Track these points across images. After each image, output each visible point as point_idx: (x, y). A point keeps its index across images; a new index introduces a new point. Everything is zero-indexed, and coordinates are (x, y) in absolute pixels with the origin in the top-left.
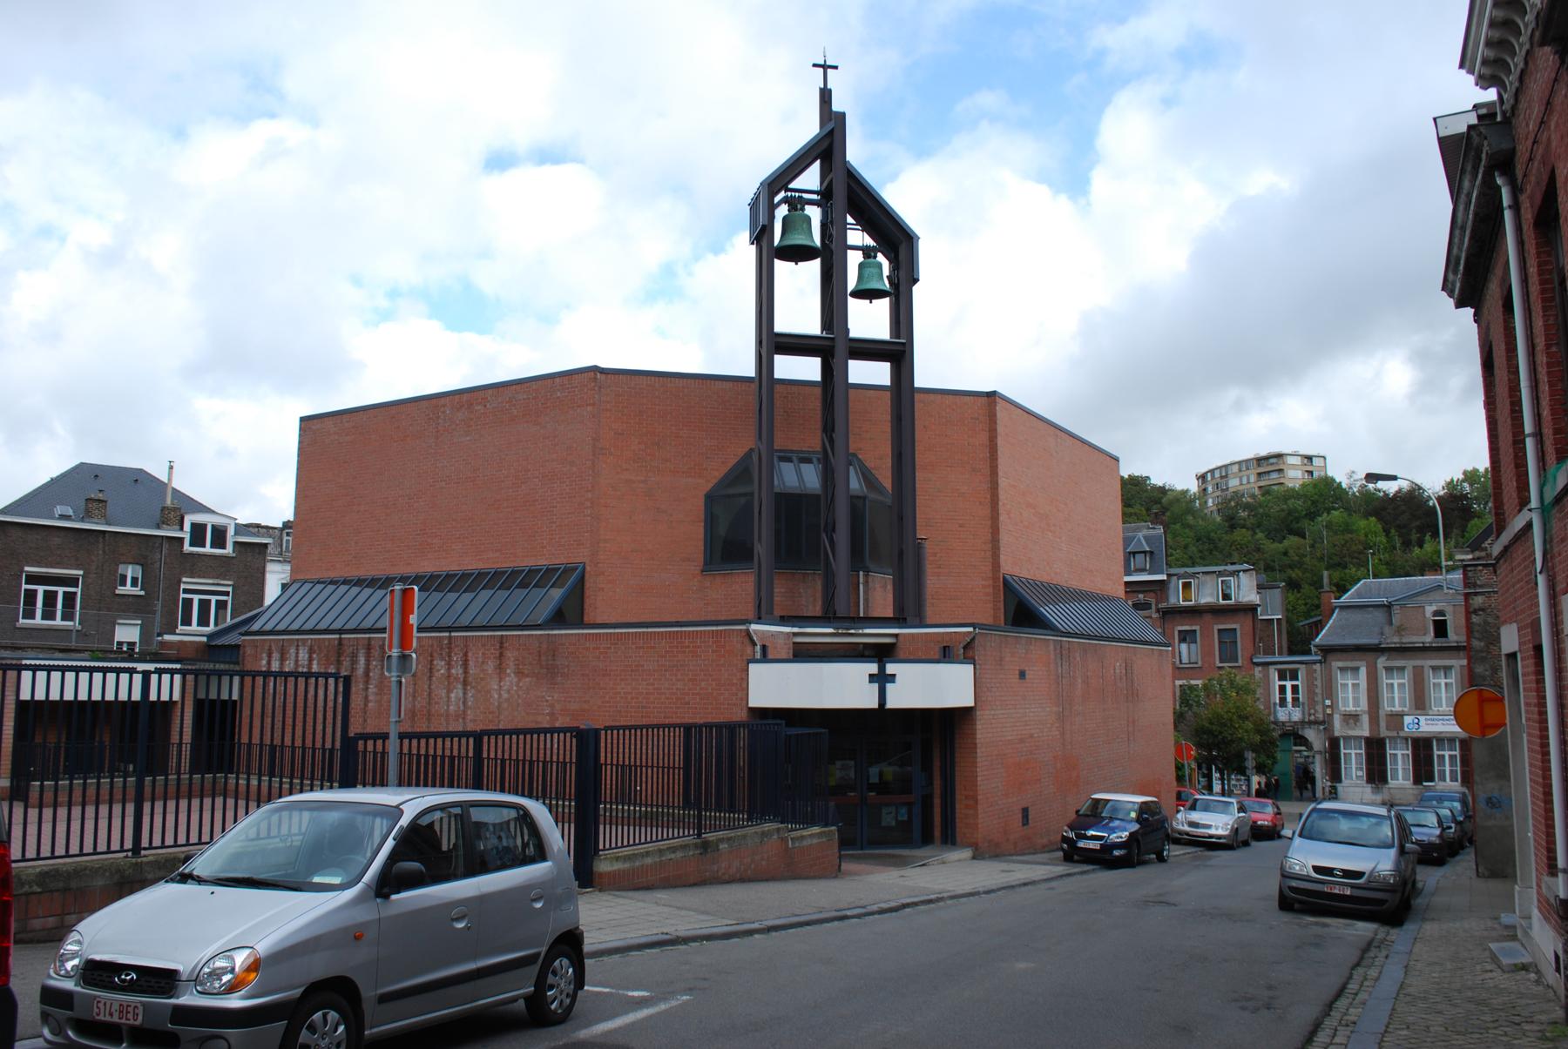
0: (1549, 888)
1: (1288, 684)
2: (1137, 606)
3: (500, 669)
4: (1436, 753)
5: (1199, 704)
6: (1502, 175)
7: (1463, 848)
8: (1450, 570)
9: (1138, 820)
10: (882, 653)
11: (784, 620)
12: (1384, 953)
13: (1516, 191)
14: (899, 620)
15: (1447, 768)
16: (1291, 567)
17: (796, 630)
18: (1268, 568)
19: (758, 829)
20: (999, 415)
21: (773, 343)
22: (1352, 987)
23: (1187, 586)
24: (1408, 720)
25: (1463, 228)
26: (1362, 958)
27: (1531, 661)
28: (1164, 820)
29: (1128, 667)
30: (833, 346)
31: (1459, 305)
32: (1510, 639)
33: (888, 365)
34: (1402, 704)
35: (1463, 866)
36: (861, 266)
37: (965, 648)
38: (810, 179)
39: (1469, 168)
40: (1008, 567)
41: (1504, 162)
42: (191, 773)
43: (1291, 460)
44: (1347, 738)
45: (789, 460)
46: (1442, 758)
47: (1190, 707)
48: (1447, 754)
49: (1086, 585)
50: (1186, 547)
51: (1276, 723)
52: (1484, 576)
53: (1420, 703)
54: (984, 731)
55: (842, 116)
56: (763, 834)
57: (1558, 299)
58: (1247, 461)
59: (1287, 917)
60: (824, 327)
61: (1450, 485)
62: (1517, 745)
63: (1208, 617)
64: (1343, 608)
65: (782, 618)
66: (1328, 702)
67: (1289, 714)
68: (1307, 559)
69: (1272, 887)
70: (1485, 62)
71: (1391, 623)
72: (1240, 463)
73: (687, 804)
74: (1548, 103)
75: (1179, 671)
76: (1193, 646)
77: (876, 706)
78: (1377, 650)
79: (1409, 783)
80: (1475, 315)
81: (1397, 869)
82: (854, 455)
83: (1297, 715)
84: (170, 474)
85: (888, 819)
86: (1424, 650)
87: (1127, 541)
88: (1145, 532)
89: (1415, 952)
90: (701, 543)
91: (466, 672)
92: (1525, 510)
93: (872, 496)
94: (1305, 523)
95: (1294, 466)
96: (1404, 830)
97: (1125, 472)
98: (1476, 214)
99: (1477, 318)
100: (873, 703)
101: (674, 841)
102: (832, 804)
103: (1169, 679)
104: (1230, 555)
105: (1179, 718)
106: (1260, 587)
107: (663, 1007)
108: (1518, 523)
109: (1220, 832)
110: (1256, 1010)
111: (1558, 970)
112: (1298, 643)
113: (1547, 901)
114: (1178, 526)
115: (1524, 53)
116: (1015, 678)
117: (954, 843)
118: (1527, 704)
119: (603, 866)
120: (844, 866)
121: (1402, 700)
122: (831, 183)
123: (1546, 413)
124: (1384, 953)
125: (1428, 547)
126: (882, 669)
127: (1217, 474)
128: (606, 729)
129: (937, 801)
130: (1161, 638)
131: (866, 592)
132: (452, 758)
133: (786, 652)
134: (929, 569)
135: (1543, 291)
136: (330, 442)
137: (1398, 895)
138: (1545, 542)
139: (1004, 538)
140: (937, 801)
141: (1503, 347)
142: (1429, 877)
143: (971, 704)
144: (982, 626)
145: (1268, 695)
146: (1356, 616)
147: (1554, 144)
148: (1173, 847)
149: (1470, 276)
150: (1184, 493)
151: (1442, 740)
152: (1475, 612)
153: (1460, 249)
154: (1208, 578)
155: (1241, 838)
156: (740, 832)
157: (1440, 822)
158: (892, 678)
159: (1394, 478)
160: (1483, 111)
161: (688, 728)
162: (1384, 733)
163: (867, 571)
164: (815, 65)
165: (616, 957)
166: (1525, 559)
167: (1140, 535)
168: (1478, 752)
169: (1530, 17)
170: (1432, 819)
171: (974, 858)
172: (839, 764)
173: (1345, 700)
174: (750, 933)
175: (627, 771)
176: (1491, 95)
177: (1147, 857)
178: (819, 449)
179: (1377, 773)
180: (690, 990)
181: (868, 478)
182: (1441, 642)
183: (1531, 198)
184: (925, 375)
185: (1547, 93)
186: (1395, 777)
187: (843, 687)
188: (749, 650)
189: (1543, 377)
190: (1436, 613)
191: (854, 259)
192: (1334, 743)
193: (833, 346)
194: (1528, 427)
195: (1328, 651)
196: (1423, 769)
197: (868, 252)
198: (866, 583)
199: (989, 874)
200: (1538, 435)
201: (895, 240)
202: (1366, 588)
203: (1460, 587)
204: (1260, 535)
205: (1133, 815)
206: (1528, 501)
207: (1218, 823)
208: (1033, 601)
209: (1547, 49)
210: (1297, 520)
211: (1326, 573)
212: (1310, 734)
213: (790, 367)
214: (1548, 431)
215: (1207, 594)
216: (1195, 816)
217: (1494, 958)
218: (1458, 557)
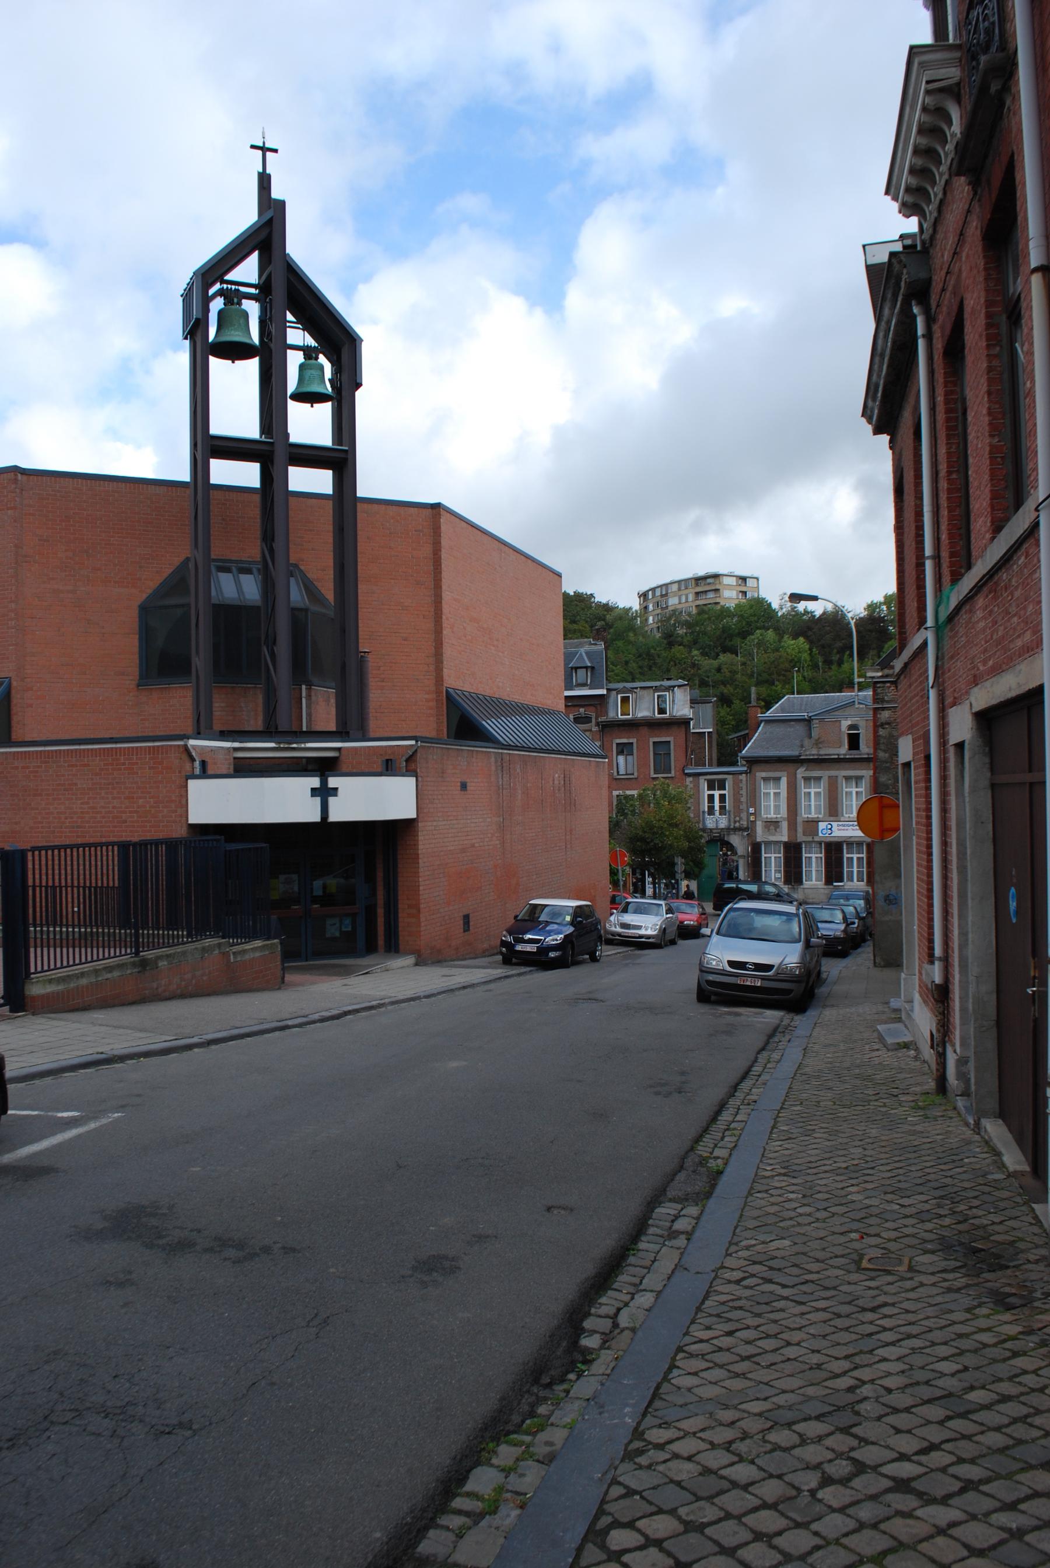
0: (927, 974)
1: (717, 794)
2: (578, 720)
4: (846, 855)
5: (633, 812)
6: (919, 303)
7: (864, 941)
8: (862, 687)
9: (572, 923)
10: (325, 767)
11: (223, 735)
12: (787, 1037)
13: (930, 321)
15: (855, 870)
17: (236, 745)
18: (703, 684)
19: (198, 945)
20: (443, 528)
21: (208, 446)
22: (757, 1069)
23: (625, 700)
24: (822, 825)
25: (882, 356)
26: (767, 1043)
27: (922, 770)
28: (598, 922)
29: (566, 777)
30: (272, 450)
31: (877, 431)
32: (906, 750)
33: (330, 472)
34: (818, 811)
35: (863, 957)
36: (302, 367)
37: (407, 761)
38: (248, 271)
39: (889, 296)
40: (451, 681)
41: (920, 292)
43: (726, 581)
44: (768, 843)
45: (228, 570)
47: (625, 815)
48: (855, 856)
49: (528, 698)
50: (627, 663)
51: (704, 830)
52: (890, 693)
53: (834, 811)
54: (426, 842)
55: (282, 204)
56: (204, 950)
57: (960, 428)
58: (686, 580)
59: (705, 1008)
60: (263, 431)
61: (872, 607)
62: (908, 847)
63: (644, 731)
64: (768, 722)
66: (752, 810)
67: (716, 822)
68: (739, 676)
69: (691, 981)
70: (908, 190)
71: (810, 736)
72: (679, 582)
73: (125, 924)
74: (961, 234)
75: (616, 781)
76: (630, 758)
78: (796, 761)
79: (821, 884)
80: (891, 442)
81: (803, 962)
82: (296, 566)
85: (332, 929)
86: (839, 761)
87: (568, 657)
88: (587, 648)
89: (815, 1034)
90: (137, 656)
92: (922, 630)
93: (315, 608)
94: (737, 641)
95: (729, 587)
96: (810, 925)
97: (570, 587)
98: (894, 342)
99: (892, 445)
100: (316, 817)
101: (109, 961)
102: (274, 917)
103: (605, 792)
104: (668, 670)
105: (614, 827)
106: (693, 702)
107: (92, 1125)
108: (916, 642)
109: (649, 932)
110: (668, 1095)
111: (932, 1047)
112: (727, 755)
113: (926, 986)
114: (620, 643)
115: (943, 182)
118: (917, 809)
119: (35, 989)
120: (288, 977)
121: (818, 807)
122: (269, 277)
123: (944, 537)
124: (787, 1037)
125: (846, 666)
126: (324, 783)
127: (658, 593)
128: (33, 849)
129: (380, 911)
130: (600, 752)
131: (308, 706)
133: (227, 767)
134: (372, 683)
135: (948, 420)
137: (803, 985)
138: (937, 659)
139: (448, 652)
140: (380, 911)
141: (912, 473)
142: (832, 968)
143: (414, 816)
144: (424, 739)
145: (698, 803)
146: (779, 730)
147: (964, 275)
148: (604, 947)
149: (887, 405)
151: (851, 843)
152: (882, 725)
153: (879, 376)
154: (645, 692)
155: (669, 937)
156: (180, 949)
157: (845, 919)
158: (334, 791)
159: (815, 598)
160: (908, 242)
161: (124, 847)
162: (801, 838)
163: (310, 685)
164: (253, 147)
165: (48, 1080)
166: (921, 675)
167: (582, 650)
168: (879, 853)
169: (950, 147)
170: (839, 916)
171: (416, 964)
172: (282, 878)
173: (768, 807)
174: (189, 1047)
175: (53, 891)
176: (912, 225)
177: (581, 958)
178: (259, 558)
180: (122, 1108)
181: (310, 589)
182: (854, 754)
183: (942, 328)
184: (370, 484)
185: (961, 223)
186: (809, 879)
187: (285, 801)
189: (944, 502)
190: (851, 727)
191: (294, 360)
192: (756, 848)
193: (272, 450)
194: (928, 551)
195: (754, 762)
196: (834, 872)
197: (309, 353)
198: (309, 696)
199: (432, 979)
200: (937, 557)
201: (338, 341)
202: (791, 704)
203: (870, 701)
204: (695, 652)
205: (568, 918)
206: (925, 622)
207: (648, 924)
208: (475, 714)
209: (963, 179)
210: (731, 637)
211: (753, 689)
212: (735, 840)
213: (226, 472)
214: (945, 554)
215: (644, 709)
216: (629, 918)
217: (881, 1039)
218: (869, 674)
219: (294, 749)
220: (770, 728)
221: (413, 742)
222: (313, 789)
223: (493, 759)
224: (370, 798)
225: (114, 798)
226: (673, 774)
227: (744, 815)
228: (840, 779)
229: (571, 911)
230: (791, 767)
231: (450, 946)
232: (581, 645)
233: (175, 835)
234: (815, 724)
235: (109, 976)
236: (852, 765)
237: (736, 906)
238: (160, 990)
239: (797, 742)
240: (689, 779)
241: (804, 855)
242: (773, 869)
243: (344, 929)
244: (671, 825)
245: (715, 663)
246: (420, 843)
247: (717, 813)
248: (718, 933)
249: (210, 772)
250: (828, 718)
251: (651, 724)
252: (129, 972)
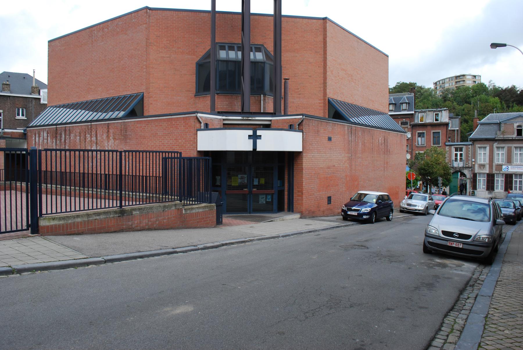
1: (459, 153)
3: (108, 137)
4: (514, 179)
11: (219, 113)
14: (273, 114)
15: (518, 185)
16: (465, 115)
17: (224, 118)
20: (328, 28)
24: (504, 167)
29: (385, 140)
37: (299, 125)
40: (331, 94)
42: (5, 181)
43: (468, 77)
44: (480, 174)
46: (516, 181)
51: (453, 168)
54: (307, 163)
58: (452, 77)
59: (425, 259)
63: (429, 128)
64: (482, 124)
65: (219, 112)
66: (473, 160)
67: (458, 164)
69: (421, 239)
71: (500, 130)
72: (449, 78)
76: (423, 138)
77: (251, 149)
78: (494, 140)
79: (503, 191)
81: (491, 235)
83: (461, 165)
84: (34, 74)
85: (262, 200)
88: (407, 95)
90: (195, 84)
91: (97, 139)
95: (469, 80)
96: (496, 209)
100: (250, 149)
106: (450, 118)
109: (420, 208)
112: (464, 138)
114: (425, 100)
116: (326, 141)
117: (293, 211)
119: (42, 223)
120: (225, 219)
121: (502, 160)
126: (255, 132)
127: (441, 82)
129: (286, 193)
131: (264, 104)
132: (146, 177)
136: (61, 49)
137: (490, 249)
139: (329, 82)
140: (286, 193)
142: (509, 231)
144: (307, 116)
150: (429, 89)
154: (430, 113)
162: (494, 171)
163: (265, 95)
167: (405, 96)
171: (301, 218)
173: (480, 159)
174: (88, 264)
179: (490, 187)
182: (519, 137)
187: (237, 141)
188: (198, 125)
192: (475, 175)
195: (475, 140)
198: (264, 100)
204: (455, 103)
205: (375, 200)
210: (469, 98)
212: (466, 172)
215: (429, 118)
219: (250, 120)
220: (482, 127)
221: (301, 117)
222: (249, 136)
223: (346, 128)
224: (273, 141)
225: (170, 139)
226: (440, 145)
227: (470, 162)
228: (512, 148)
229: (375, 197)
230: (491, 143)
231: (319, 210)
232: (405, 95)
233: (192, 156)
234: (502, 125)
235: (98, 217)
236: (518, 142)
237: (451, 198)
238: (133, 226)
239: (494, 132)
240: (447, 147)
241: (496, 179)
242: (482, 184)
243: (267, 200)
244: (436, 164)
245: (462, 107)
246: (304, 163)
247: (459, 161)
248: (438, 214)
249: (210, 127)
250: (508, 123)
251: (432, 125)
252: (112, 216)
